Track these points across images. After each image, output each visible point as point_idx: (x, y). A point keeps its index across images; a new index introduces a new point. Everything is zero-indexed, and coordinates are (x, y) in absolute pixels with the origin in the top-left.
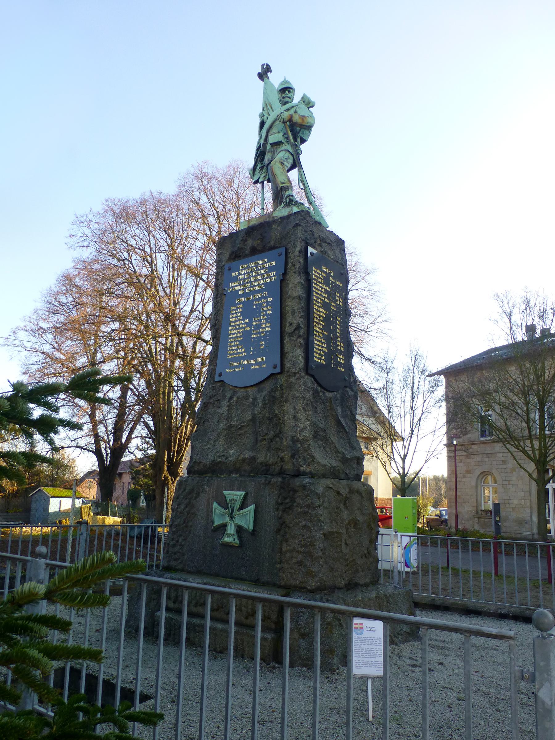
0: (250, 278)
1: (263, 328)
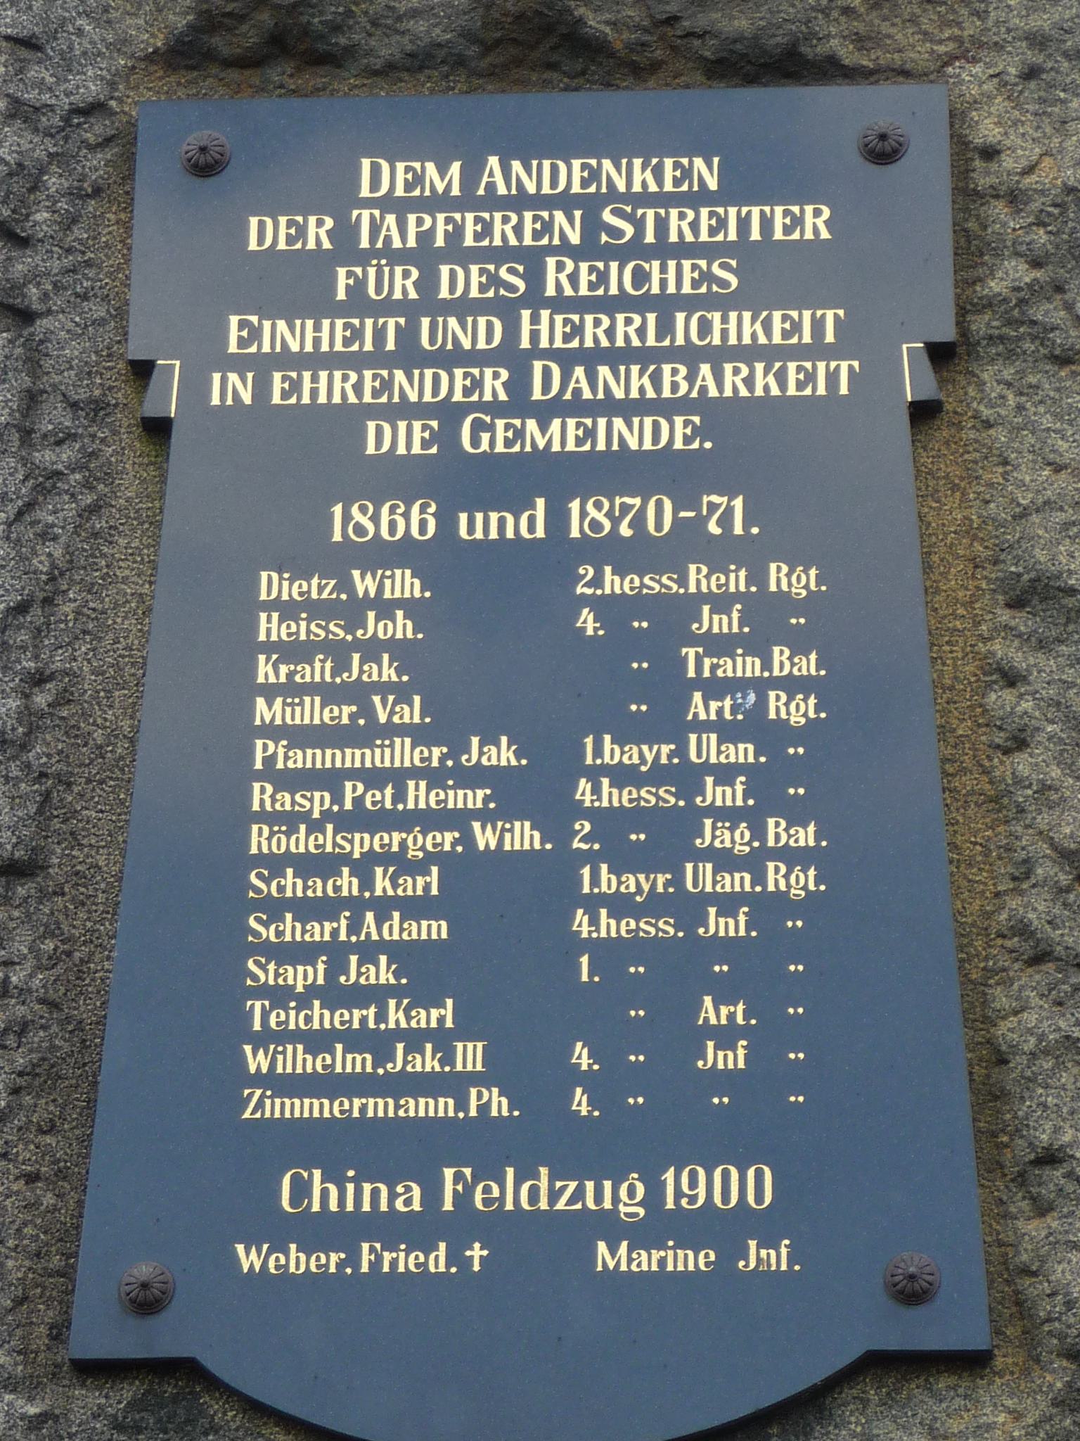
1: (725, 861)
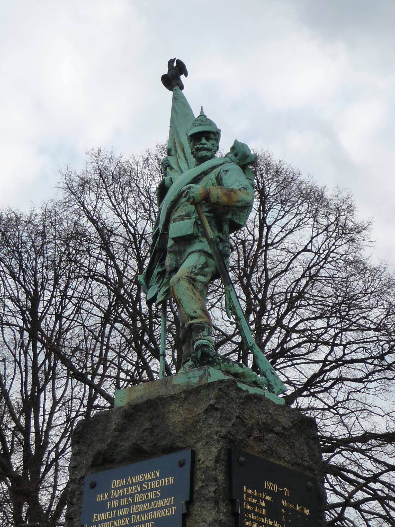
0: (129, 506)
